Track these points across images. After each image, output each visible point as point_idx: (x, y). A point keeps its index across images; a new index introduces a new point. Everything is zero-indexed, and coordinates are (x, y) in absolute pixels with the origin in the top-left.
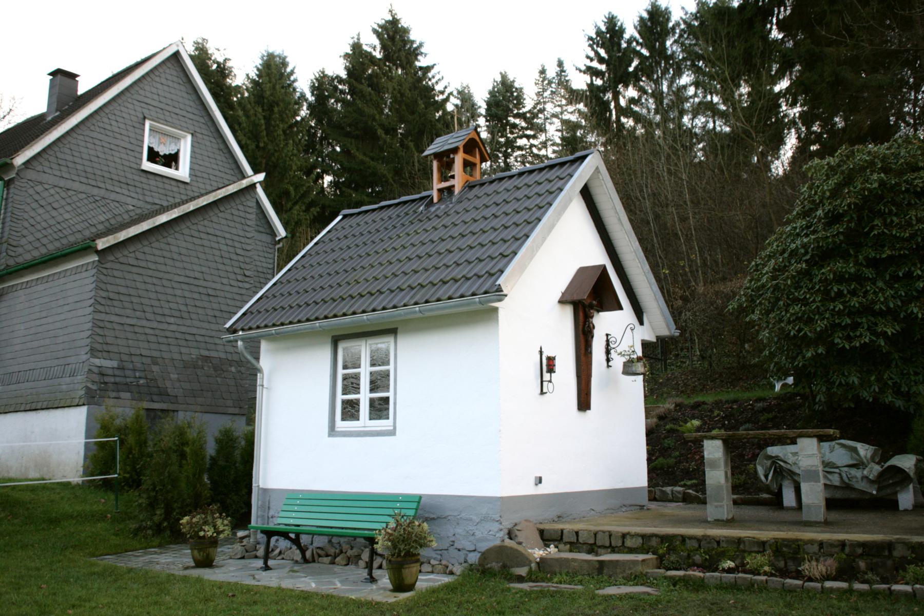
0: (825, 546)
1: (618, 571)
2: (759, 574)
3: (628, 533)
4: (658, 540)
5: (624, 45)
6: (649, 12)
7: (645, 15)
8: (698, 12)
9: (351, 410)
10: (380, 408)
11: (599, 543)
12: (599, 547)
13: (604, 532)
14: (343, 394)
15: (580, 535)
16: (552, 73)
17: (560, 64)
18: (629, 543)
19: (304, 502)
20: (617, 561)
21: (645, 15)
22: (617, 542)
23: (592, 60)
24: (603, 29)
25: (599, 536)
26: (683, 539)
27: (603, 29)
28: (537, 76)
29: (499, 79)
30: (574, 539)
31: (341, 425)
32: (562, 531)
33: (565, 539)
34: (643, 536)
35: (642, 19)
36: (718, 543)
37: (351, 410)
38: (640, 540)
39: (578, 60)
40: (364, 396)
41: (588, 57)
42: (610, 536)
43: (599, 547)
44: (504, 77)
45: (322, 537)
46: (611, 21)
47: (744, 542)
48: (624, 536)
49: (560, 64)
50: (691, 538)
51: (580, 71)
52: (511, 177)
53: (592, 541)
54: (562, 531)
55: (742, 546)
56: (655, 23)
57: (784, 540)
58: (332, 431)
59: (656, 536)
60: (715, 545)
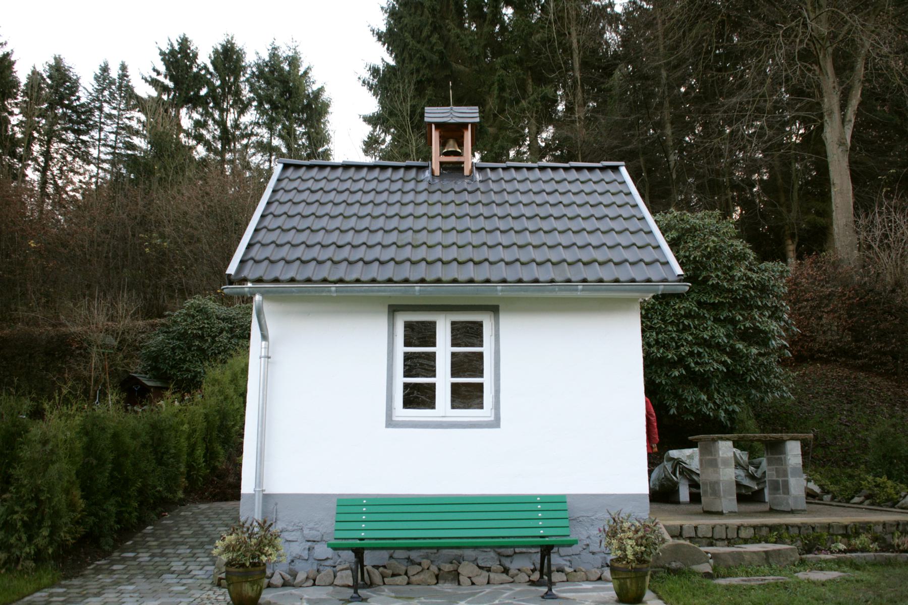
0: (887, 526)
1: (782, 559)
2: (868, 551)
3: (742, 525)
4: (767, 529)
5: (195, 70)
6: (223, 46)
7: (219, 48)
8: (270, 61)
9: (419, 397)
10: (467, 396)
11: (717, 536)
12: (717, 540)
13: (721, 525)
14: (405, 376)
15: (699, 529)
16: (114, 73)
17: (123, 68)
18: (744, 534)
19: (547, 507)
20: (779, 550)
21: (219, 48)
22: (732, 534)
23: (159, 73)
24: (177, 47)
25: (716, 530)
26: (787, 527)
27: (177, 47)
28: (98, 72)
29: (52, 62)
30: (693, 534)
31: (402, 413)
32: (681, 527)
33: (685, 534)
34: (755, 527)
35: (216, 52)
36: (813, 528)
37: (419, 397)
38: (752, 530)
39: (144, 69)
40: (443, 380)
41: (154, 70)
42: (727, 528)
43: (717, 540)
44: (58, 60)
45: (377, 553)
46: (184, 43)
47: (833, 526)
48: (739, 528)
49: (123, 68)
50: (793, 526)
51: (146, 81)
52: (322, 167)
53: (710, 535)
54: (681, 527)
55: (831, 530)
56: (228, 58)
57: (860, 523)
58: (390, 423)
59: (766, 526)
60: (811, 531)
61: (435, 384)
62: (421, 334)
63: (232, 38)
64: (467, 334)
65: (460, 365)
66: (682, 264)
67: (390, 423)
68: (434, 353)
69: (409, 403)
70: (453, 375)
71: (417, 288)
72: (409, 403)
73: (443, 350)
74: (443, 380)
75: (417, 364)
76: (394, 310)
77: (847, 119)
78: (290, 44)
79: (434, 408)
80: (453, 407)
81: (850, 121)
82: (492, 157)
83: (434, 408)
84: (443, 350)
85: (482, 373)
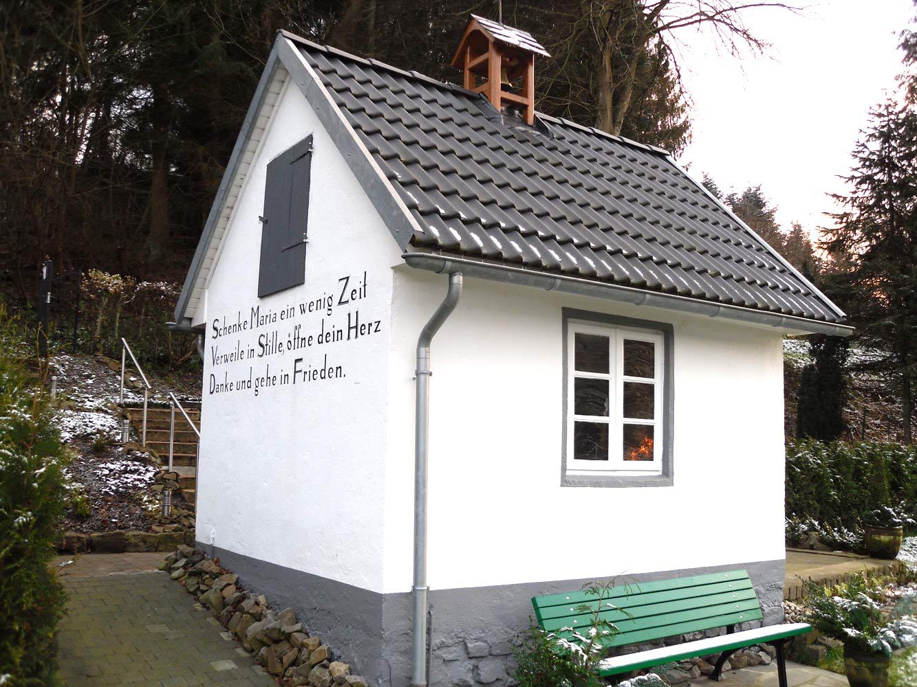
9: (590, 443)
10: (637, 442)
40: (616, 420)
58: (566, 481)
61: (607, 425)
62: (591, 354)
63: (758, 189)
64: (638, 359)
65: (638, 400)
66: (51, 300)
67: (566, 481)
68: (607, 382)
69: (580, 453)
70: (626, 415)
71: (648, 296)
72: (580, 453)
73: (617, 378)
74: (616, 420)
75: (590, 397)
76: (569, 314)
77: (618, 121)
78: (690, 118)
79: (606, 458)
80: (625, 459)
81: (620, 123)
82: (821, 284)
83: (606, 458)
84: (617, 378)
85: (653, 413)
